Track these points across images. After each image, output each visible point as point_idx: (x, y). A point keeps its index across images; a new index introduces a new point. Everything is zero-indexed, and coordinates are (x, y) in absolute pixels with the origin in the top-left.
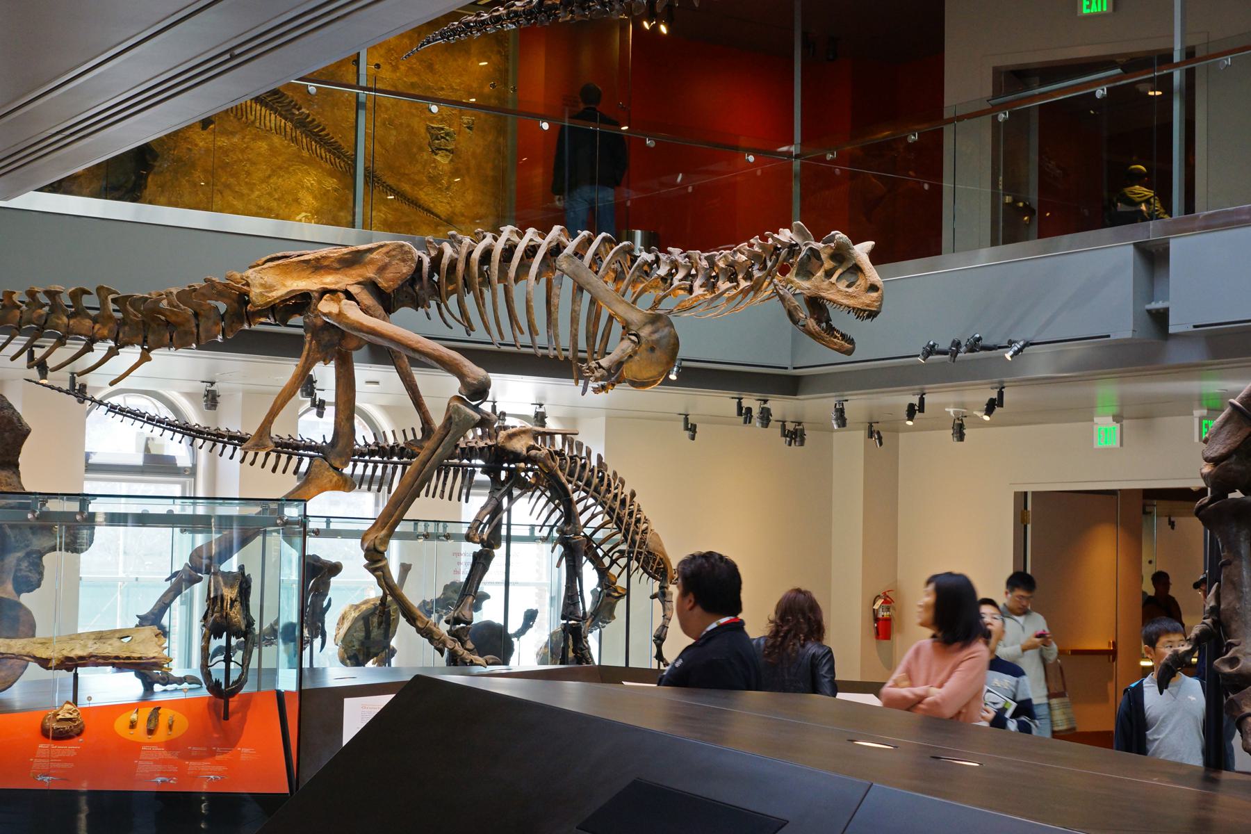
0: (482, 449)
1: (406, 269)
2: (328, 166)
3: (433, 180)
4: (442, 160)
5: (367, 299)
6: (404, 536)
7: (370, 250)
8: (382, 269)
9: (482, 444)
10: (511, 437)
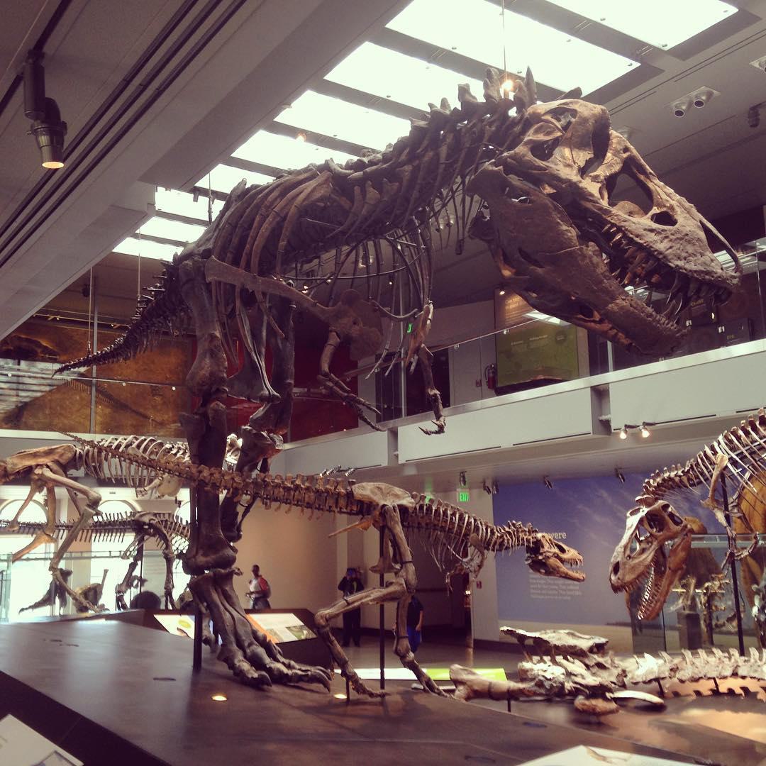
0: (129, 521)
1: (70, 455)
2: (106, 403)
3: (154, 407)
4: (158, 399)
5: (55, 467)
6: (66, 558)
7: (57, 448)
8: (61, 455)
9: (129, 519)
10: (141, 516)
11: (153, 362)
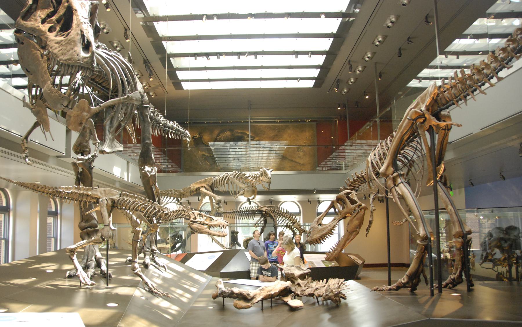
3: (299, 157)
5: (207, 187)
7: (207, 179)
8: (209, 182)
11: (298, 136)
